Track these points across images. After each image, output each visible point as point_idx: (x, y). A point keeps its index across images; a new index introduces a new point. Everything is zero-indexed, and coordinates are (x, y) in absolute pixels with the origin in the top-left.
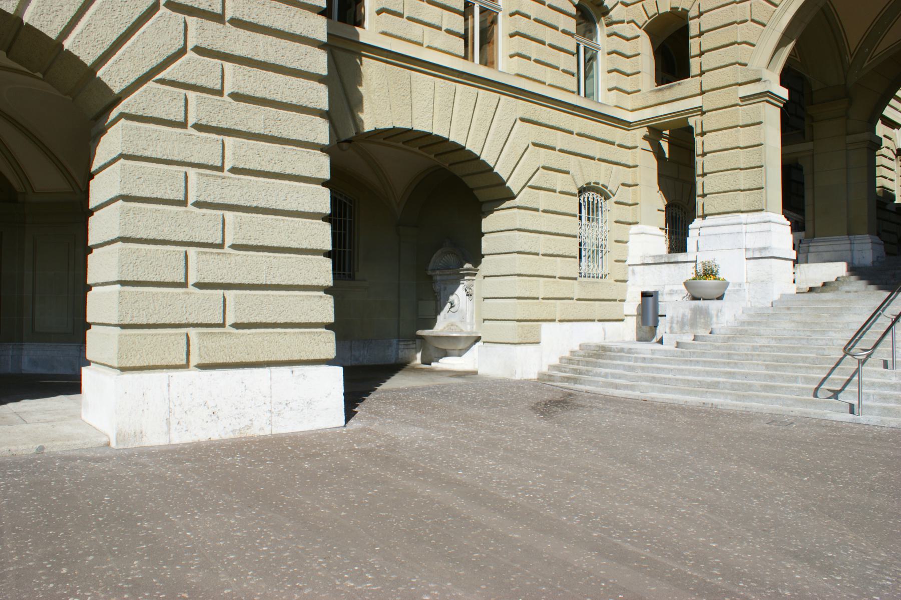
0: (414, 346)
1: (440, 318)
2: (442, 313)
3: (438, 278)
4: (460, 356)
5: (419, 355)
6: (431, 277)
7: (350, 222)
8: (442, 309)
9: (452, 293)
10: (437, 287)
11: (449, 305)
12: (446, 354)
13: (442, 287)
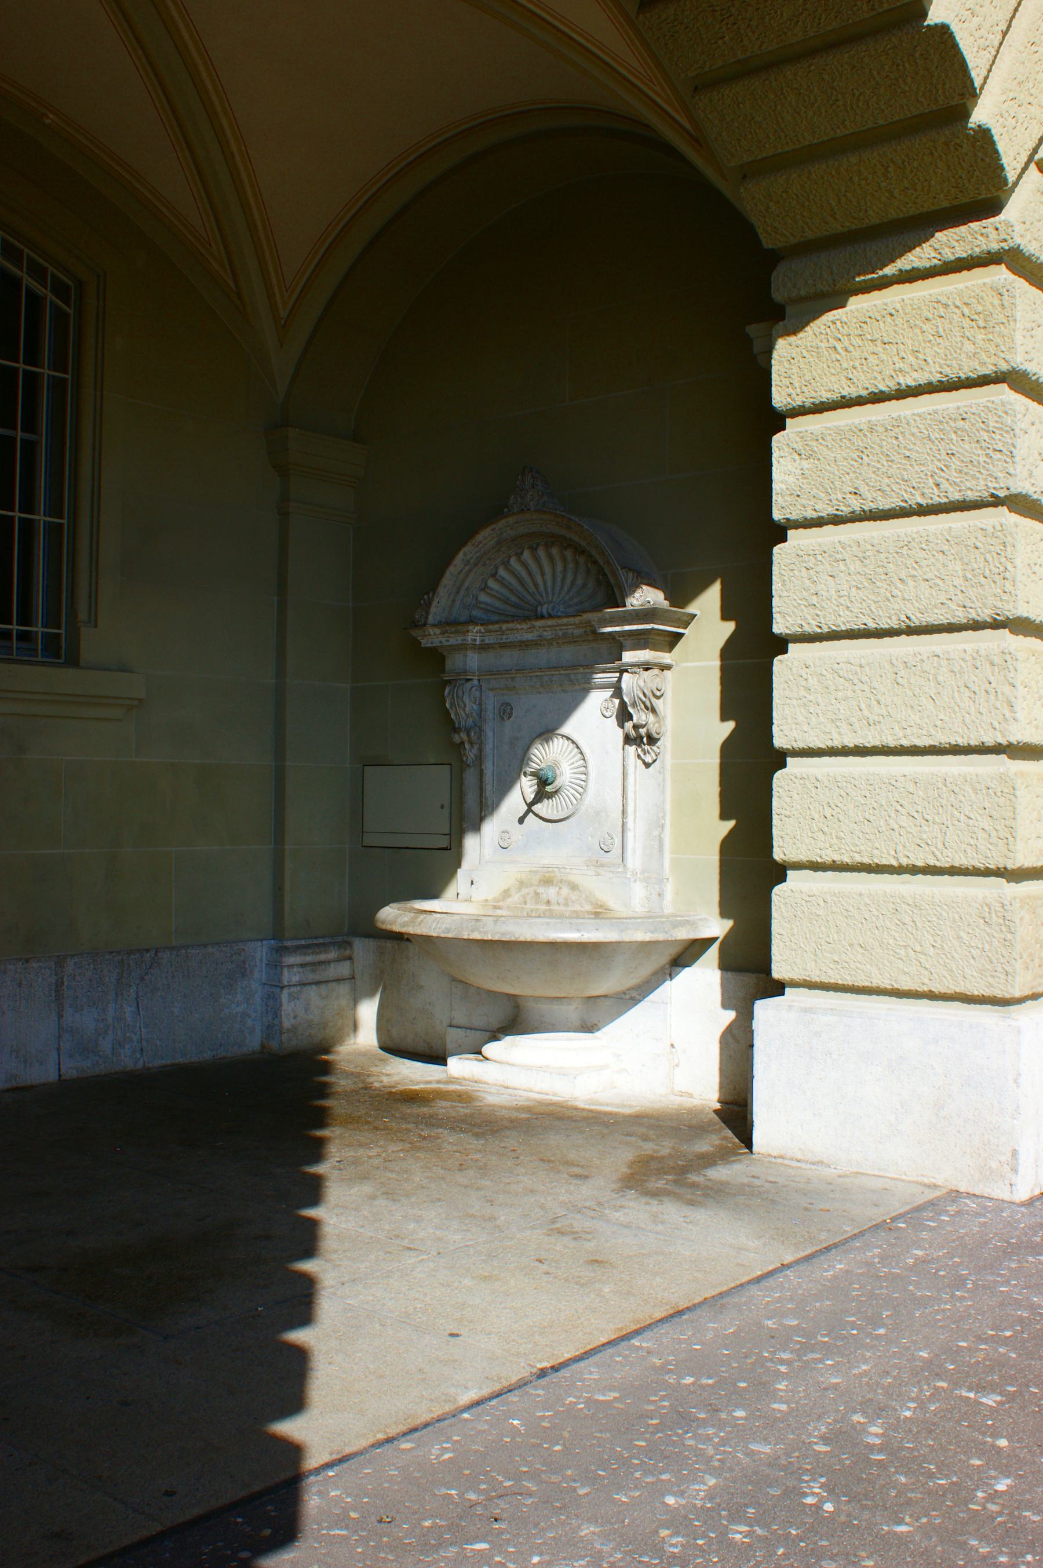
0: (344, 969)
1: (479, 848)
2: (491, 828)
3: (473, 661)
4: (588, 1027)
5: (368, 1012)
6: (436, 657)
7: (58, 386)
8: (485, 808)
9: (547, 733)
10: (464, 706)
11: (527, 786)
12: (514, 1020)
13: (491, 702)
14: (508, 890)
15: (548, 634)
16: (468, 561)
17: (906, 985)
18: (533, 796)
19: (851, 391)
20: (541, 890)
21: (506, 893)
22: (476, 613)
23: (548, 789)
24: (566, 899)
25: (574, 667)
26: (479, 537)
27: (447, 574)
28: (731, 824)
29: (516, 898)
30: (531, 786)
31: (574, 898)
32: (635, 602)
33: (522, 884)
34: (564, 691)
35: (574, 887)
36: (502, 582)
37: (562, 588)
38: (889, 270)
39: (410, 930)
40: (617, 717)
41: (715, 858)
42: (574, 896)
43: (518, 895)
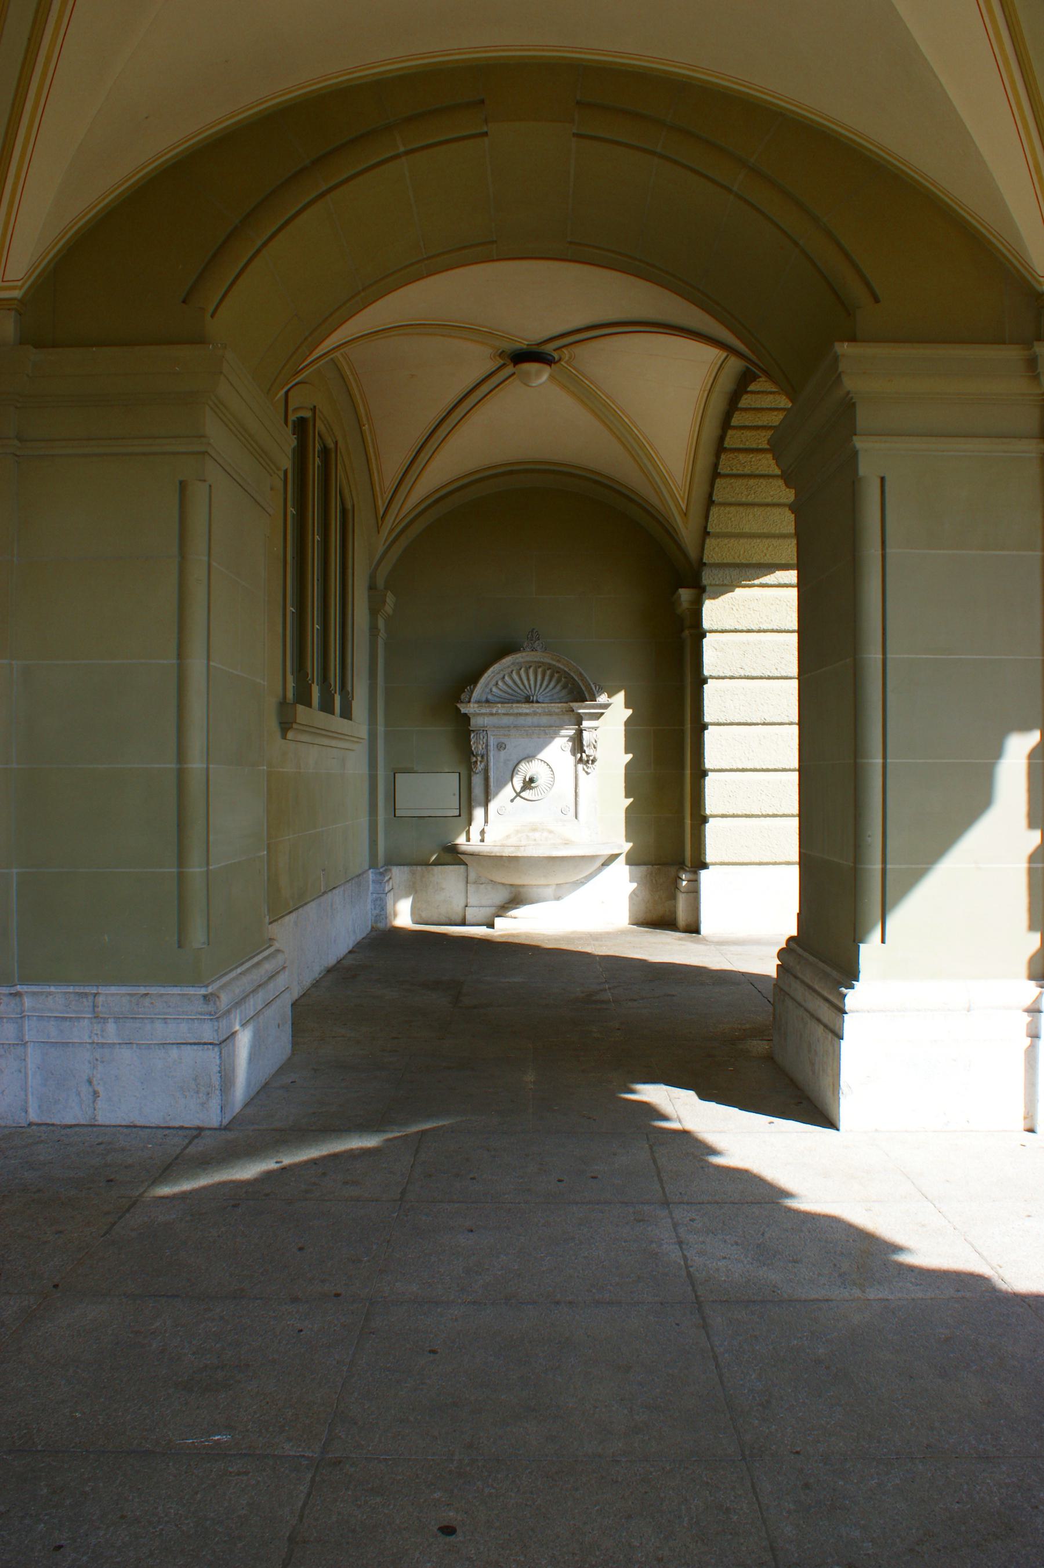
9: (529, 757)
13: (492, 741)
15: (539, 711)
17: (765, 860)
19: (740, 627)
20: (530, 834)
22: (490, 697)
25: (551, 726)
26: (504, 661)
28: (631, 800)
35: (551, 832)
36: (505, 683)
37: (541, 685)
38: (756, 582)
39: (519, 855)
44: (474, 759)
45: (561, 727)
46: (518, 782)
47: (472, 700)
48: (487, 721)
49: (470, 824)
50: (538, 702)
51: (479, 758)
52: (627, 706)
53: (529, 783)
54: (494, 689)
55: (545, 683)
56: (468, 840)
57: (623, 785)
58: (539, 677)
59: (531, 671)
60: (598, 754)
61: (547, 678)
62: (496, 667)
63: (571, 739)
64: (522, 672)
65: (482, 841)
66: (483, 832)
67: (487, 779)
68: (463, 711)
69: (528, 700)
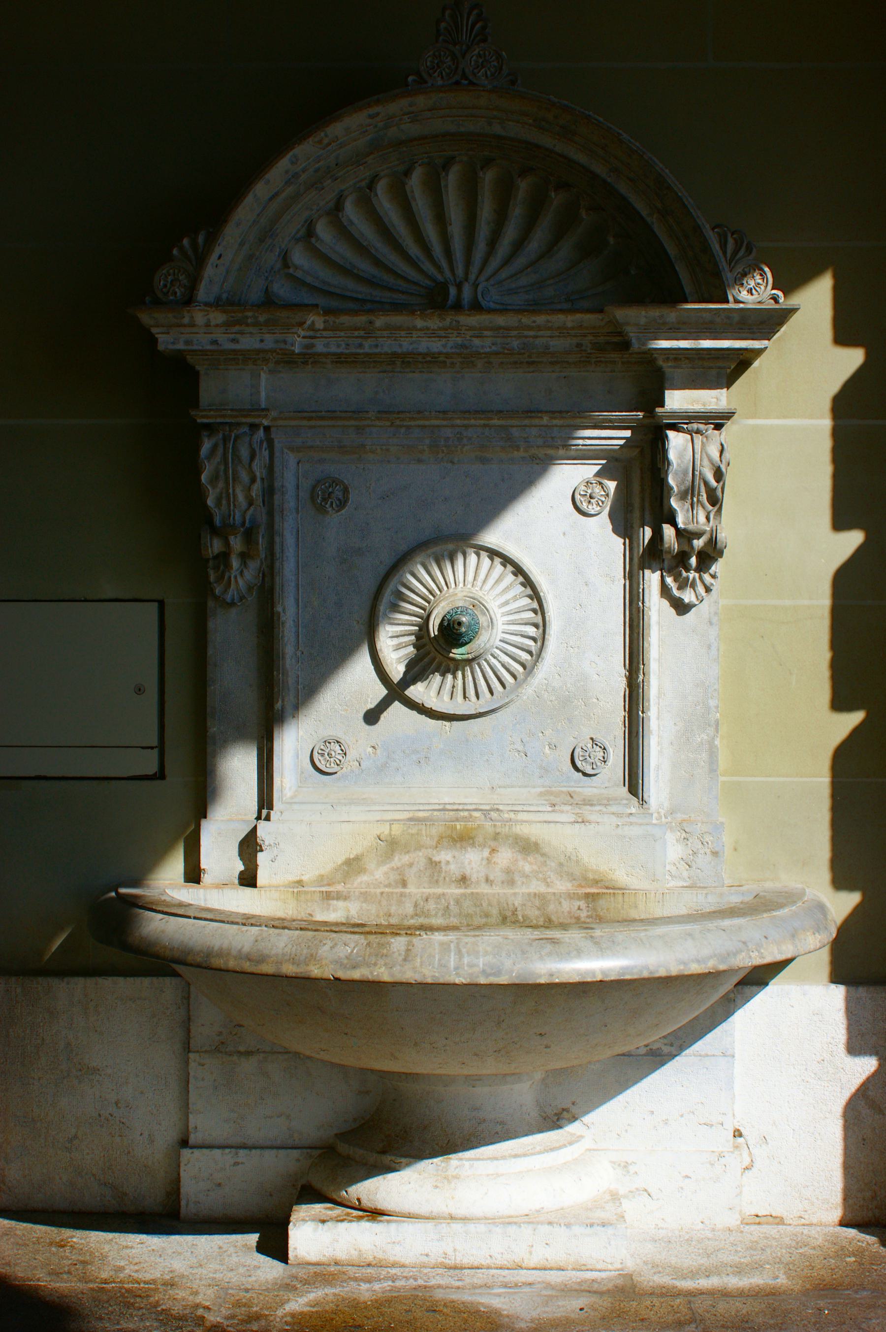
4: (554, 1118)
6: (182, 374)
9: (452, 538)
13: (292, 475)
14: (357, 859)
15: (483, 344)
16: (296, 175)
18: (402, 669)
20: (444, 856)
21: (353, 866)
22: (282, 289)
23: (458, 653)
24: (508, 871)
25: (531, 412)
26: (336, 129)
27: (249, 199)
28: (856, 718)
29: (378, 874)
30: (398, 648)
31: (527, 868)
32: (744, 295)
33: (391, 846)
34: (483, 460)
35: (528, 847)
36: (344, 232)
37: (492, 244)
39: (383, 973)
40: (611, 516)
41: (823, 781)
42: (527, 865)
43: (385, 868)
44: (217, 546)
45: (579, 415)
46: (394, 645)
47: (203, 293)
48: (267, 386)
49: (202, 813)
50: (476, 307)
51: (237, 543)
52: (843, 335)
53: (443, 646)
54: (299, 257)
55: (510, 233)
56: (193, 875)
57: (822, 655)
58: (486, 211)
59: (452, 179)
60: (730, 528)
61: (517, 212)
62: (304, 155)
63: (615, 465)
64: (415, 182)
65: (248, 879)
66: (249, 847)
67: (268, 628)
68: (166, 341)
69: (437, 299)
